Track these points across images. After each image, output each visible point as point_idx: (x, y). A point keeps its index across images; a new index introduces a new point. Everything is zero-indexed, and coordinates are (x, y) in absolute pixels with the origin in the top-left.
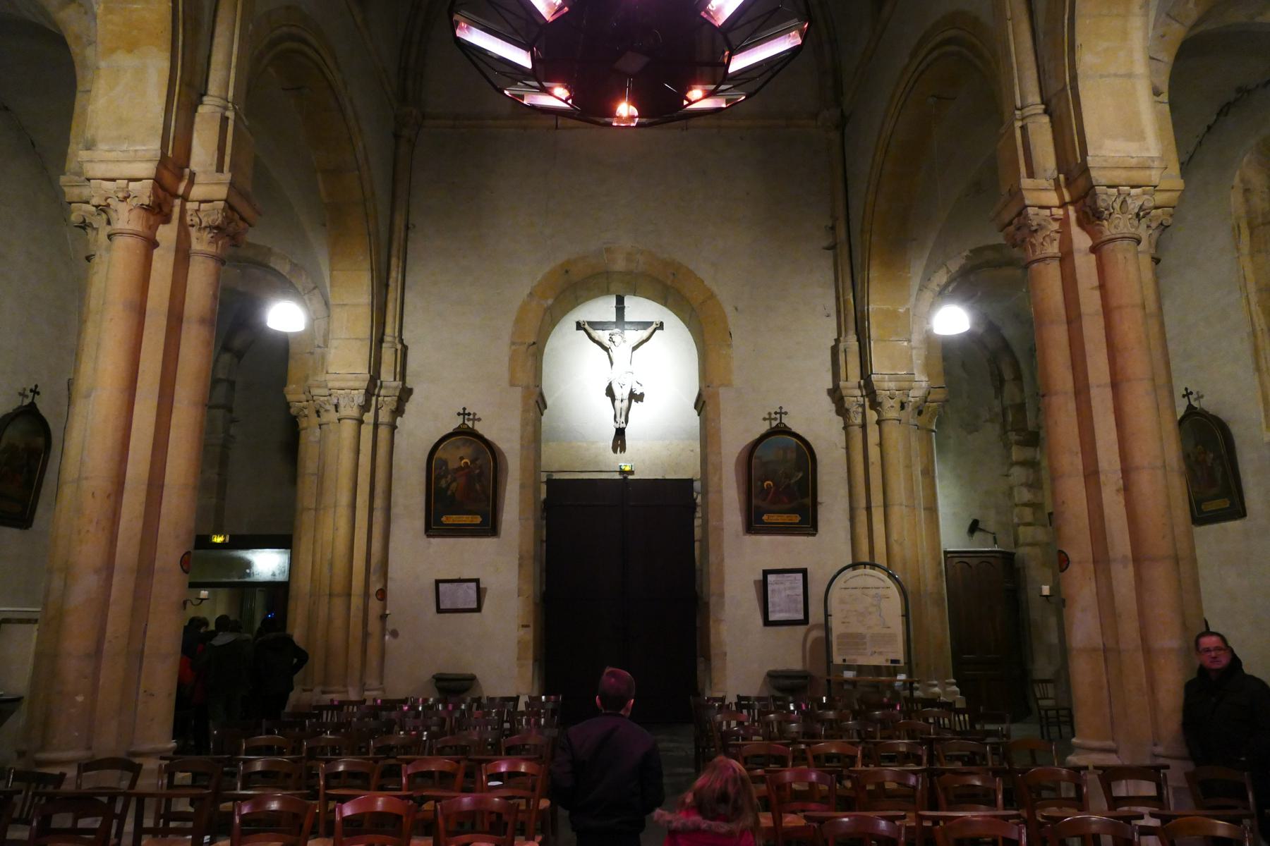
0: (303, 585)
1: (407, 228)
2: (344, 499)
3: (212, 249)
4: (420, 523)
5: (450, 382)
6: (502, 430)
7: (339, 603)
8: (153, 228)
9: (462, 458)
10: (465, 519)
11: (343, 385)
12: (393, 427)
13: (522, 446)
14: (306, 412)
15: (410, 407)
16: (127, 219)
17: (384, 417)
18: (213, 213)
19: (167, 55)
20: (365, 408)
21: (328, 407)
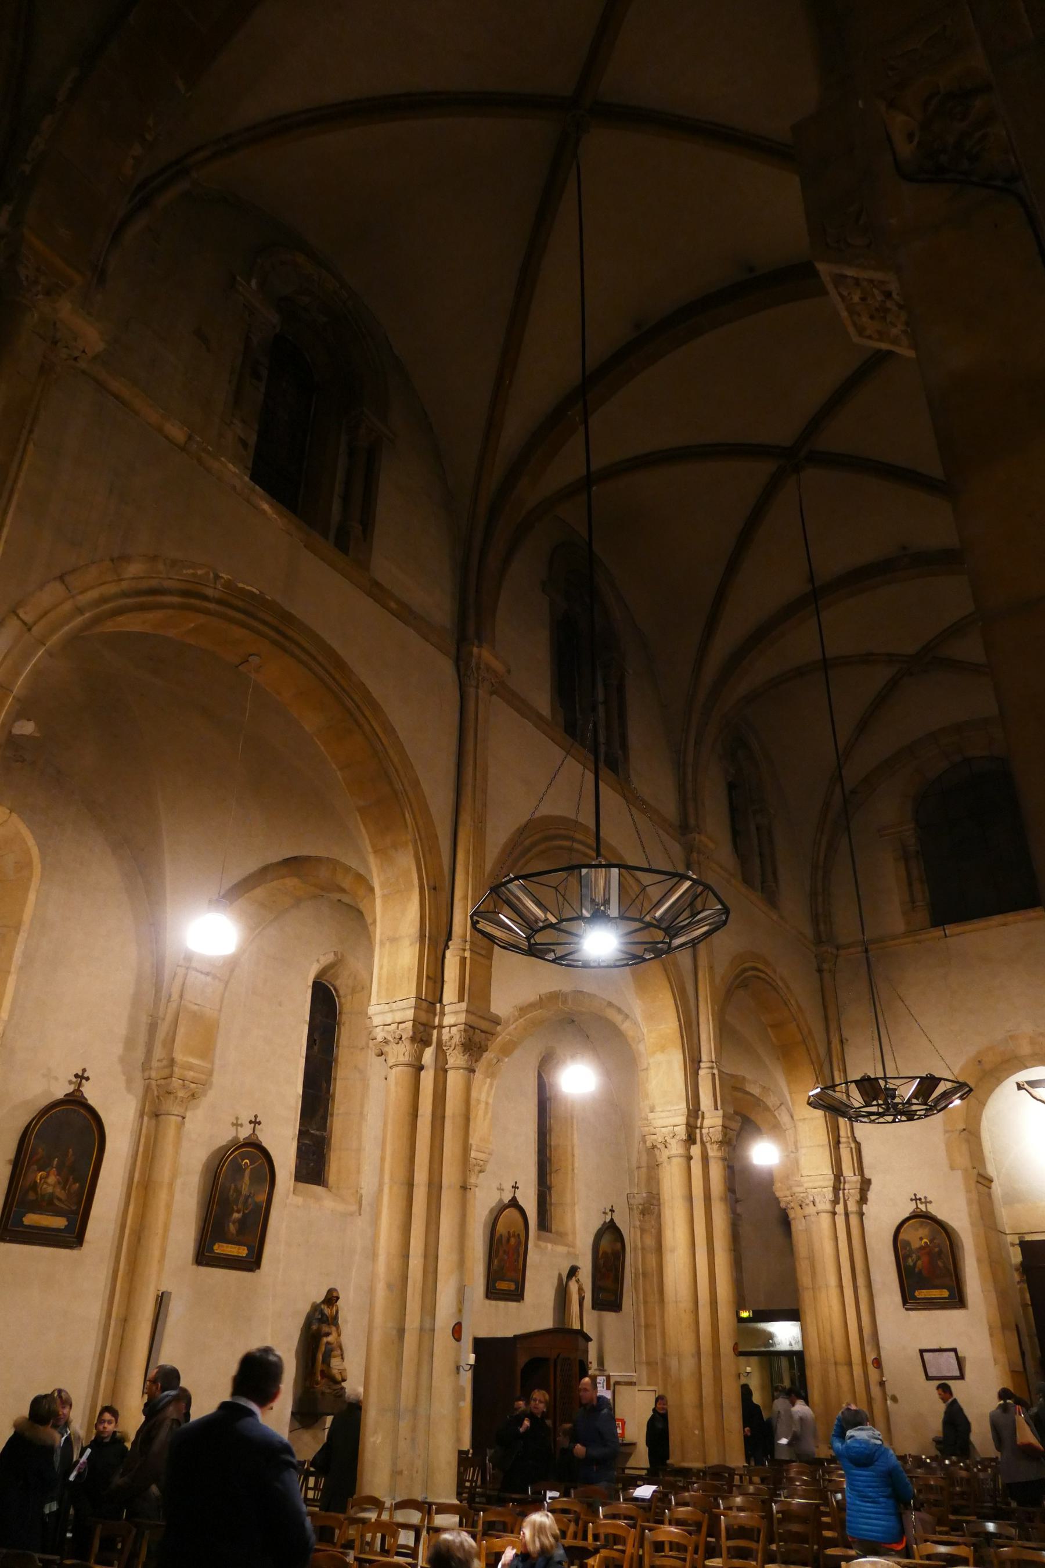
0: (813, 1356)
1: (842, 1042)
2: (833, 1281)
3: (719, 1154)
4: (898, 1298)
5: (905, 1166)
6: (954, 1210)
7: (843, 1370)
8: (688, 1150)
9: (921, 1239)
10: (935, 1293)
11: (817, 1184)
12: (861, 1215)
13: (972, 1224)
14: (792, 1205)
15: (871, 1195)
16: (676, 1148)
17: (852, 1207)
18: (716, 1134)
19: (681, 1051)
20: (835, 1201)
21: (807, 1202)
